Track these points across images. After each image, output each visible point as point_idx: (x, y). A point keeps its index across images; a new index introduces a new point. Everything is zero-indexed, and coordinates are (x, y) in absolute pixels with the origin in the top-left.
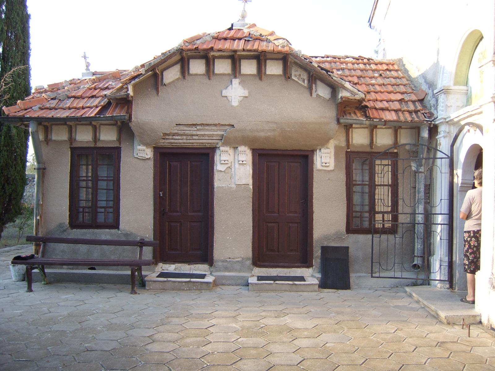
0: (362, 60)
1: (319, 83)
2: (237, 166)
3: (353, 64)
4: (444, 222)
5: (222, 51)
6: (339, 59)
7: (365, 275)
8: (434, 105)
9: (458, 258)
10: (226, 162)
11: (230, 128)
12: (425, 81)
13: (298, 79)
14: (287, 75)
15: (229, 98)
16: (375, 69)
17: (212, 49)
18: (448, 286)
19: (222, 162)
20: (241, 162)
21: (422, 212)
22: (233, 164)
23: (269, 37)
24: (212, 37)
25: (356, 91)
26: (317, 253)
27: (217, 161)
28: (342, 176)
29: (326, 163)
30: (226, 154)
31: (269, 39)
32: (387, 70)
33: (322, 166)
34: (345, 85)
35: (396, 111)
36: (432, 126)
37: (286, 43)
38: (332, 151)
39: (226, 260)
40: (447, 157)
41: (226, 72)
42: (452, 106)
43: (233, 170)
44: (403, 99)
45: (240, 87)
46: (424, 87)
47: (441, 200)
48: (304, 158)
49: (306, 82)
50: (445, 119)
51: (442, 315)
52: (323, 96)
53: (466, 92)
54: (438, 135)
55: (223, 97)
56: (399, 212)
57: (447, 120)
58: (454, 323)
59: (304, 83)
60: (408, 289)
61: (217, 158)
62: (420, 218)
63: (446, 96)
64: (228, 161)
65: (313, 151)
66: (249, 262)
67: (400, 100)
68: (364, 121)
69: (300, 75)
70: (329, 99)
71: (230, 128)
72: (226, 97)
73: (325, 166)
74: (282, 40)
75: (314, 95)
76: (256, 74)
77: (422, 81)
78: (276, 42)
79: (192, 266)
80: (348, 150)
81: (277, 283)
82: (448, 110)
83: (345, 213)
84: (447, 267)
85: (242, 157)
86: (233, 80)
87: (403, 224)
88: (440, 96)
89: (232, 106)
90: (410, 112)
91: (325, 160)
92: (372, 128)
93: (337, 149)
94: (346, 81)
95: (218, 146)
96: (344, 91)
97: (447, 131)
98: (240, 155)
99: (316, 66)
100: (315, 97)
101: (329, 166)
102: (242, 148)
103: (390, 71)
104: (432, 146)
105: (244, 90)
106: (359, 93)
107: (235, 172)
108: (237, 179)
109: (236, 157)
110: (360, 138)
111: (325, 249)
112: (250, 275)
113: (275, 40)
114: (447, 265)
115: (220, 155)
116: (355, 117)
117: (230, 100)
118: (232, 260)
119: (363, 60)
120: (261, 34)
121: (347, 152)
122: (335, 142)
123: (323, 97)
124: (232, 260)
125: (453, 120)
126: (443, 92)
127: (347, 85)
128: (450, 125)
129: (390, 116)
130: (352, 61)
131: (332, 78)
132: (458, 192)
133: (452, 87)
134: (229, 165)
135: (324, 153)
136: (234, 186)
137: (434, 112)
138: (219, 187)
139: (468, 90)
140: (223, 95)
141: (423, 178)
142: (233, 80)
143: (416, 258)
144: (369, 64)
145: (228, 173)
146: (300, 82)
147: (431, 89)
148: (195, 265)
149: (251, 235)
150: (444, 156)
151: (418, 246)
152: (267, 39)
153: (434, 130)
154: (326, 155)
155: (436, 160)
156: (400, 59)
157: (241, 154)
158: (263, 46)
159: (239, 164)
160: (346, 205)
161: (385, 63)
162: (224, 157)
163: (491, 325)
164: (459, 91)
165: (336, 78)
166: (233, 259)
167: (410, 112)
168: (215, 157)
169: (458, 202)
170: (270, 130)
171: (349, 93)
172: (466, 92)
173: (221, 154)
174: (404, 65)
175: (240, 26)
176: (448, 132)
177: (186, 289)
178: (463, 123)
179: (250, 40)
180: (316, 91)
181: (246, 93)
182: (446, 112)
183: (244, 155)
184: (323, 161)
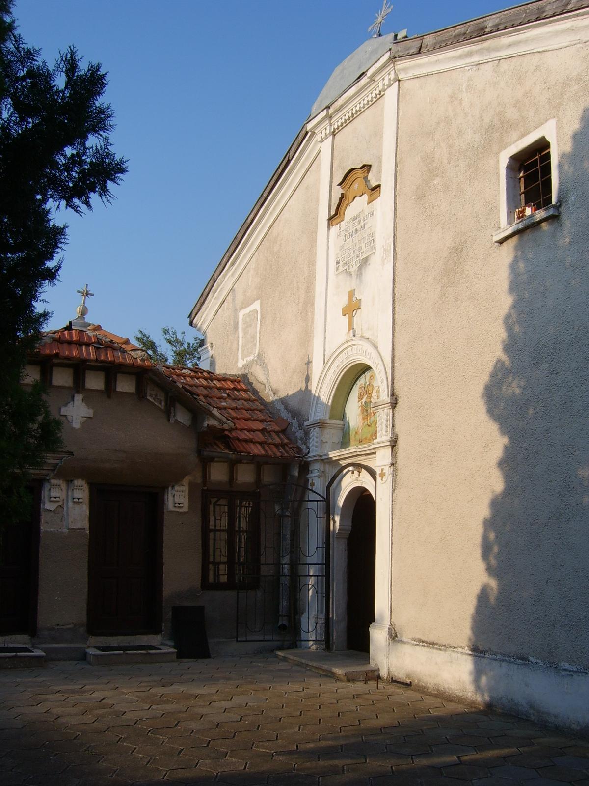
0: (201, 373)
1: (178, 406)
2: (70, 504)
3: (192, 378)
4: (319, 573)
5: (69, 358)
6: (173, 369)
7: (224, 640)
8: (301, 438)
9: (335, 614)
10: (57, 499)
11: (68, 456)
12: (286, 408)
13: (155, 400)
14: (140, 394)
15: (69, 418)
16: (220, 387)
17: (57, 355)
18: (324, 646)
19: (52, 499)
20: (76, 500)
21: (288, 562)
22: (65, 500)
23: (123, 346)
24: (52, 338)
25: (225, 419)
26: (168, 615)
27: (44, 497)
28: (197, 520)
29: (179, 504)
30: (57, 489)
31: (124, 349)
32: (234, 389)
33: (175, 507)
34: (213, 412)
35: (261, 443)
36: (303, 463)
37: (146, 355)
38: (186, 488)
39: (54, 628)
40: (322, 499)
41: (67, 385)
42: (327, 442)
43: (65, 509)
44: (265, 429)
45: (84, 404)
46: (285, 415)
47: (317, 548)
48: (153, 499)
49: (163, 404)
50: (321, 456)
51: (339, 671)
52: (182, 422)
53: (343, 427)
54: (309, 473)
55: (61, 415)
56: (261, 563)
57: (323, 458)
58: (354, 680)
59: (161, 404)
60: (280, 654)
61: (45, 494)
62: (286, 570)
63: (322, 430)
64: (59, 498)
65: (164, 489)
66: (82, 630)
67: (262, 430)
68: (231, 455)
69: (156, 395)
70: (190, 426)
71: (68, 456)
72: (66, 416)
73: (179, 507)
74: (141, 351)
75: (172, 421)
76: (103, 389)
77: (281, 407)
78: (133, 353)
79: (8, 638)
80: (204, 488)
81: (127, 654)
82: (322, 445)
83: (200, 565)
84: (324, 625)
85: (78, 494)
86: (76, 395)
87: (264, 576)
88: (312, 429)
89: (73, 429)
90: (277, 446)
91: (178, 499)
92: (233, 465)
93: (192, 486)
94: (214, 407)
95: (48, 478)
96: (211, 419)
97: (322, 470)
98: (75, 490)
99: (181, 386)
100: (173, 422)
101: (182, 507)
102: (78, 482)
103: (238, 390)
104: (304, 486)
105: (89, 409)
106: (229, 421)
107: (67, 512)
108: (70, 520)
109: (70, 493)
110: (218, 474)
111: (178, 611)
112: (85, 646)
113: (132, 350)
114: (324, 622)
115: (50, 490)
116: (219, 450)
117: (71, 421)
118: (62, 627)
119: (202, 373)
120: (112, 341)
121: (203, 490)
122: (190, 478)
123: (183, 424)
124: (62, 627)
125: (331, 458)
126: (319, 426)
127: (215, 412)
128: (325, 463)
129: (257, 450)
130: (190, 374)
131: (199, 403)
132: (335, 539)
133: (329, 421)
134: (60, 503)
135: (178, 492)
136: (66, 530)
137: (304, 447)
138: (46, 531)
139: (344, 425)
140: (62, 413)
141: (289, 523)
142: (76, 395)
143: (280, 618)
144: (212, 380)
145: (58, 513)
146: (156, 404)
147: (296, 418)
148: (10, 636)
149: (86, 594)
150: (318, 498)
151: (284, 603)
152: (121, 347)
153: (305, 467)
154: (180, 493)
155: (304, 503)
156: (245, 375)
157: (76, 489)
158: (119, 357)
159: (74, 502)
160: (201, 555)
161: (230, 380)
162: (55, 492)
163: (392, 678)
164: (335, 426)
165: (202, 403)
166: (63, 626)
167: (277, 446)
168: (42, 492)
169: (335, 550)
170: (117, 461)
171: (216, 422)
172: (343, 427)
173: (52, 489)
174: (251, 384)
175: (81, 326)
176: (323, 472)
177: (9, 667)
178: (343, 463)
179: (101, 348)
180: (174, 416)
181: (89, 412)
182: (321, 448)
183: (80, 490)
184: (177, 501)
